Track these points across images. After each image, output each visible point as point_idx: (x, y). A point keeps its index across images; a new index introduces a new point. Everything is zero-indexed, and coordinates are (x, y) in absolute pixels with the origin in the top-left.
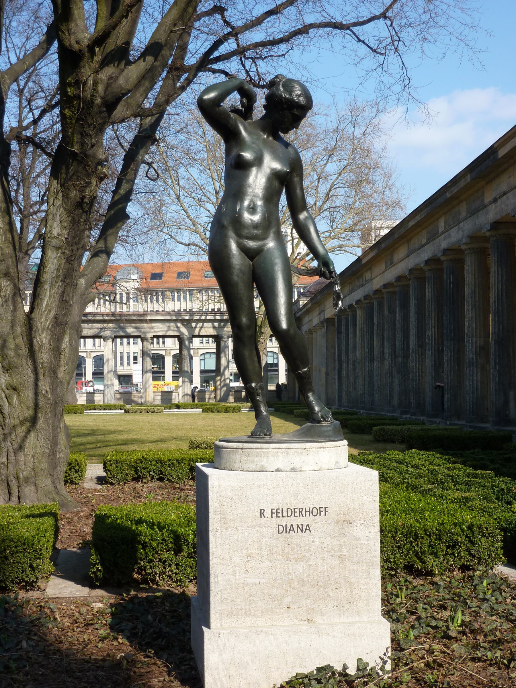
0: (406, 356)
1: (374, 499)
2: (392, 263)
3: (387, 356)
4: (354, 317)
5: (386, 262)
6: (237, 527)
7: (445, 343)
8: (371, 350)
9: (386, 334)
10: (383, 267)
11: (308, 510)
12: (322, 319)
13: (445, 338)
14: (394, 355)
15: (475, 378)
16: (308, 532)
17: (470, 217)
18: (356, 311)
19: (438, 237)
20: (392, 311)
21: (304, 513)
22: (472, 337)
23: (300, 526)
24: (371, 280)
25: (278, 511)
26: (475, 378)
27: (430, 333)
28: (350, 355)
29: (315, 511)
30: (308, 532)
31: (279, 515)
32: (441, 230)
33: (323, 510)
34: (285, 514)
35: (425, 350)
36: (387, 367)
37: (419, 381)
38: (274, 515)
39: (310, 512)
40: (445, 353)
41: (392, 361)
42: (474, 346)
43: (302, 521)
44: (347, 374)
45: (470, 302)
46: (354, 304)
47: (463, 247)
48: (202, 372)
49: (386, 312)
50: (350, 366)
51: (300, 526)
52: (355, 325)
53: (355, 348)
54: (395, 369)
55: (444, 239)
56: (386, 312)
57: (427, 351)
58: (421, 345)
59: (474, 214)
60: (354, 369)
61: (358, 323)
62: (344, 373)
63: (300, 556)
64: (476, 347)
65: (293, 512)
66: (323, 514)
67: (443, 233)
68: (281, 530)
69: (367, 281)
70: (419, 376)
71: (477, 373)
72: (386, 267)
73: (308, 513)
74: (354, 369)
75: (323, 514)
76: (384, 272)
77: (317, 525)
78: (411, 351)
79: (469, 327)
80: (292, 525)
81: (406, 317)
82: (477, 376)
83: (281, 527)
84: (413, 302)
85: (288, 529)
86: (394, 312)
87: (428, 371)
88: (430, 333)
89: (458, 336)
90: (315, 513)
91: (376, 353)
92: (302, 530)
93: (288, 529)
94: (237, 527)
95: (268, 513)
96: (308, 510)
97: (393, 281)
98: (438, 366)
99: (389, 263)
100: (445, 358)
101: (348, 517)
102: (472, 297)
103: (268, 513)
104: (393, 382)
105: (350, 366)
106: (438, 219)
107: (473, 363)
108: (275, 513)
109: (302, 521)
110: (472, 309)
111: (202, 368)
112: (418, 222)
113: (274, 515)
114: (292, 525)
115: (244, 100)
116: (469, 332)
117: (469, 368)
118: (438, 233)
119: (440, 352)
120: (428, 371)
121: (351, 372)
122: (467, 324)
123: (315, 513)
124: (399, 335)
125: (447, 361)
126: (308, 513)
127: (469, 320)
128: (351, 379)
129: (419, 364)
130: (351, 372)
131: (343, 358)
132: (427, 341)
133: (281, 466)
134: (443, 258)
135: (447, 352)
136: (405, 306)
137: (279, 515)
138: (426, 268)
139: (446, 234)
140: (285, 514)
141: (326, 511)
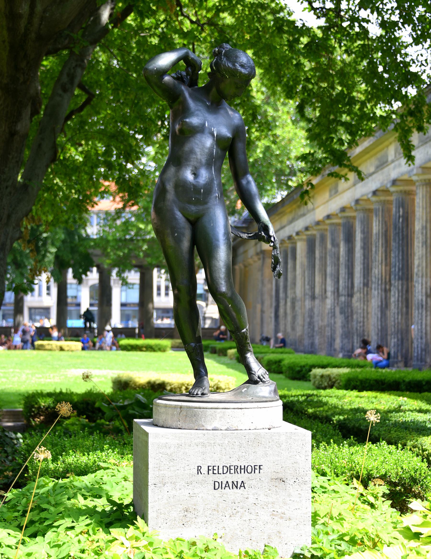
0: (351, 295)
1: (307, 458)
2: (337, 192)
3: (329, 294)
4: (294, 250)
5: (330, 191)
6: (174, 483)
7: (393, 282)
8: (313, 288)
9: (329, 269)
10: (327, 195)
11: (243, 467)
12: (259, 250)
13: (392, 277)
14: (337, 292)
15: (424, 322)
16: (242, 488)
17: (422, 145)
18: (295, 243)
19: (387, 166)
20: (335, 244)
21: (239, 470)
22: (422, 277)
23: (236, 483)
24: (314, 209)
25: (215, 468)
26: (424, 322)
27: (377, 270)
28: (289, 292)
29: (249, 470)
30: (242, 488)
31: (215, 472)
32: (390, 159)
33: (258, 467)
34: (221, 471)
35: (371, 289)
36: (329, 306)
37: (364, 322)
38: (211, 472)
39: (245, 469)
40: (392, 293)
41: (335, 299)
42: (424, 286)
43: (239, 478)
44: (285, 313)
45: (421, 239)
46: (294, 234)
47: (414, 178)
48: (123, 305)
49: (329, 246)
50: (289, 304)
51: (236, 483)
52: (294, 258)
53: (294, 284)
54: (337, 310)
55: (394, 168)
56: (329, 246)
57: (373, 291)
58: (366, 284)
59: (426, 143)
60: (293, 307)
61: (298, 257)
62: (281, 311)
63: (234, 512)
64: (426, 288)
65: (229, 469)
66: (257, 471)
67: (393, 161)
68: (218, 486)
69: (309, 211)
70: (364, 317)
71: (426, 316)
72: (331, 196)
73: (243, 471)
74: (293, 307)
75: (257, 471)
76: (327, 201)
77: (251, 482)
78: (356, 289)
79: (418, 266)
80: (227, 482)
81: (350, 252)
82: (426, 320)
83: (217, 484)
84: (358, 236)
85: (224, 486)
86: (338, 246)
87: (373, 313)
88: (377, 270)
89: (406, 275)
90: (249, 470)
91: (317, 290)
92: (237, 487)
93: (224, 486)
94: (174, 483)
95: (204, 470)
96: (243, 467)
97: (338, 211)
98: (384, 307)
99: (333, 192)
100: (392, 299)
101: (280, 476)
102: (422, 233)
103: (204, 470)
104: (335, 323)
105: (289, 304)
106: (387, 147)
107: (422, 306)
108: (211, 469)
109: (239, 478)
110: (422, 246)
111: (124, 300)
112: (367, 148)
113: (211, 472)
114: (227, 482)
115: (190, 70)
116: (418, 271)
117: (418, 310)
118: (387, 161)
119: (387, 291)
120: (373, 313)
121: (289, 311)
122: (416, 262)
123: (249, 470)
124: (343, 271)
125: (394, 302)
126: (243, 471)
127: (419, 259)
128: (289, 318)
129: (364, 304)
130: (289, 311)
131: (282, 295)
132: (374, 279)
133: (218, 426)
134: (392, 189)
135: (395, 292)
136: (350, 239)
137: (215, 472)
138: (374, 199)
139: (397, 163)
140: (221, 471)
141: (260, 469)
